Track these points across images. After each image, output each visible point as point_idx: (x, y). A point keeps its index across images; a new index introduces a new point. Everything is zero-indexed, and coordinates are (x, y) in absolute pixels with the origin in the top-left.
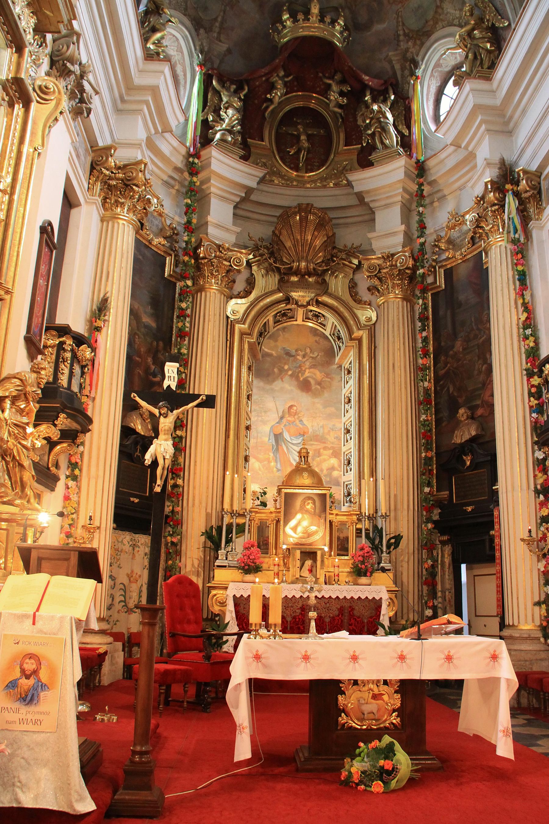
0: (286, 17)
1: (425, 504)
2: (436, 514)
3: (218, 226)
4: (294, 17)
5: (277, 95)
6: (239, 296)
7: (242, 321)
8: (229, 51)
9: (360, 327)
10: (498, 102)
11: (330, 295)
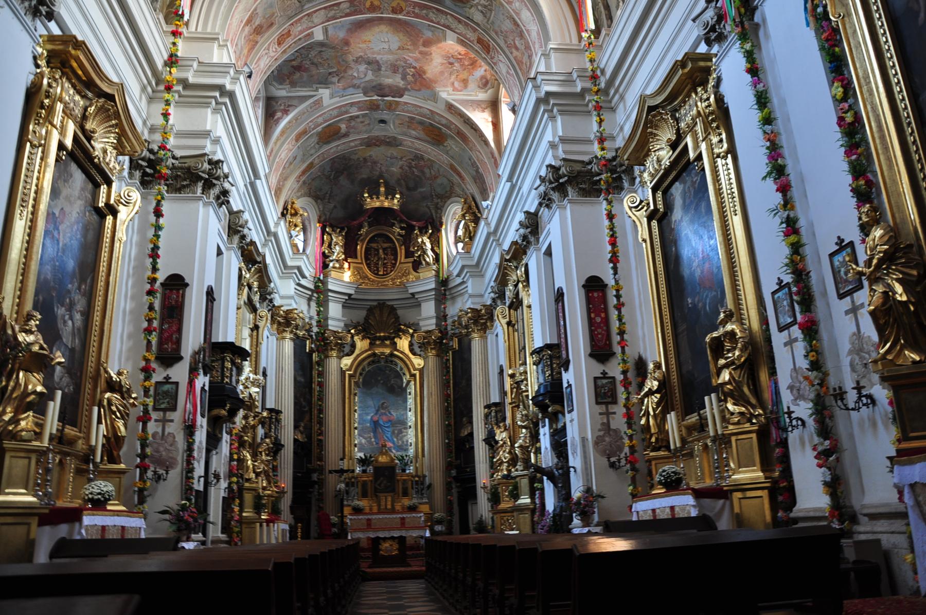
0: (366, 195)
1: (449, 466)
2: (454, 473)
3: (334, 319)
4: (371, 197)
5: (363, 231)
6: (348, 355)
7: (349, 370)
8: (335, 207)
9: (415, 369)
10: (474, 262)
11: (398, 351)
